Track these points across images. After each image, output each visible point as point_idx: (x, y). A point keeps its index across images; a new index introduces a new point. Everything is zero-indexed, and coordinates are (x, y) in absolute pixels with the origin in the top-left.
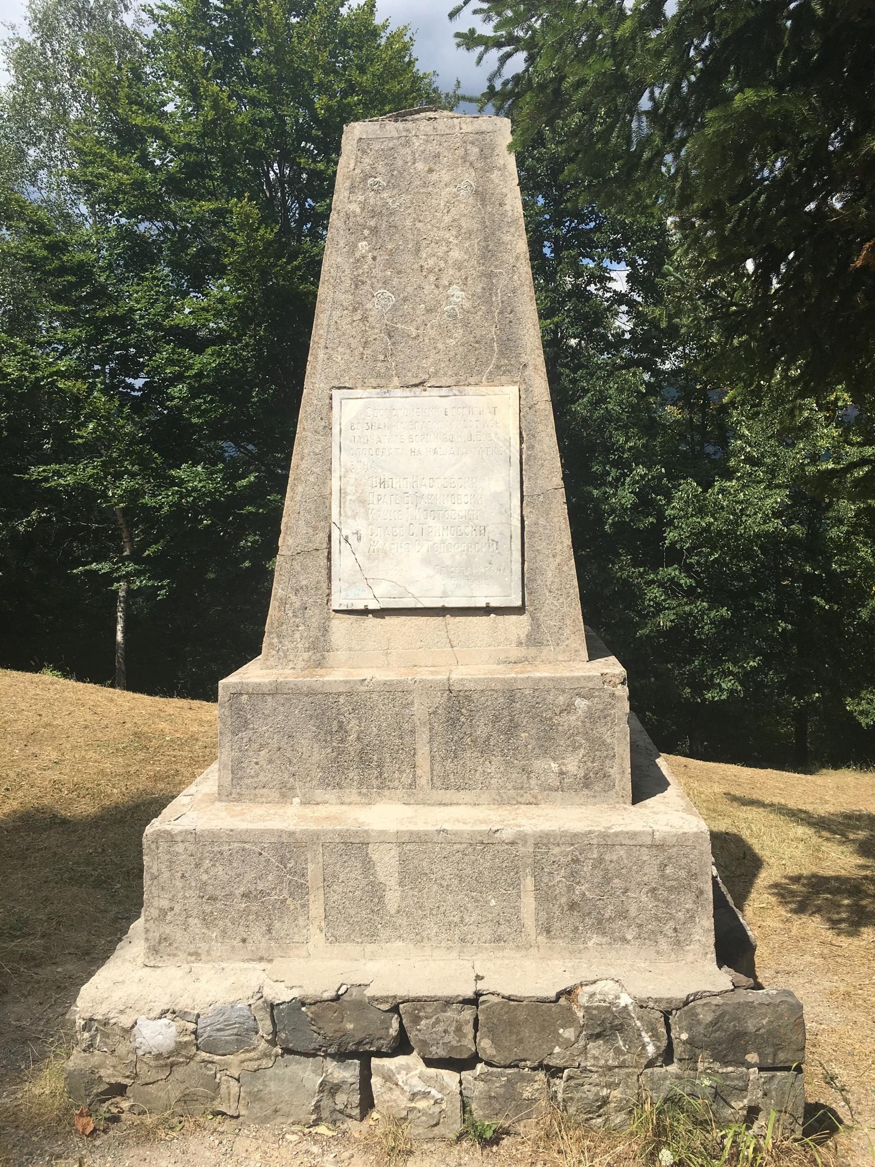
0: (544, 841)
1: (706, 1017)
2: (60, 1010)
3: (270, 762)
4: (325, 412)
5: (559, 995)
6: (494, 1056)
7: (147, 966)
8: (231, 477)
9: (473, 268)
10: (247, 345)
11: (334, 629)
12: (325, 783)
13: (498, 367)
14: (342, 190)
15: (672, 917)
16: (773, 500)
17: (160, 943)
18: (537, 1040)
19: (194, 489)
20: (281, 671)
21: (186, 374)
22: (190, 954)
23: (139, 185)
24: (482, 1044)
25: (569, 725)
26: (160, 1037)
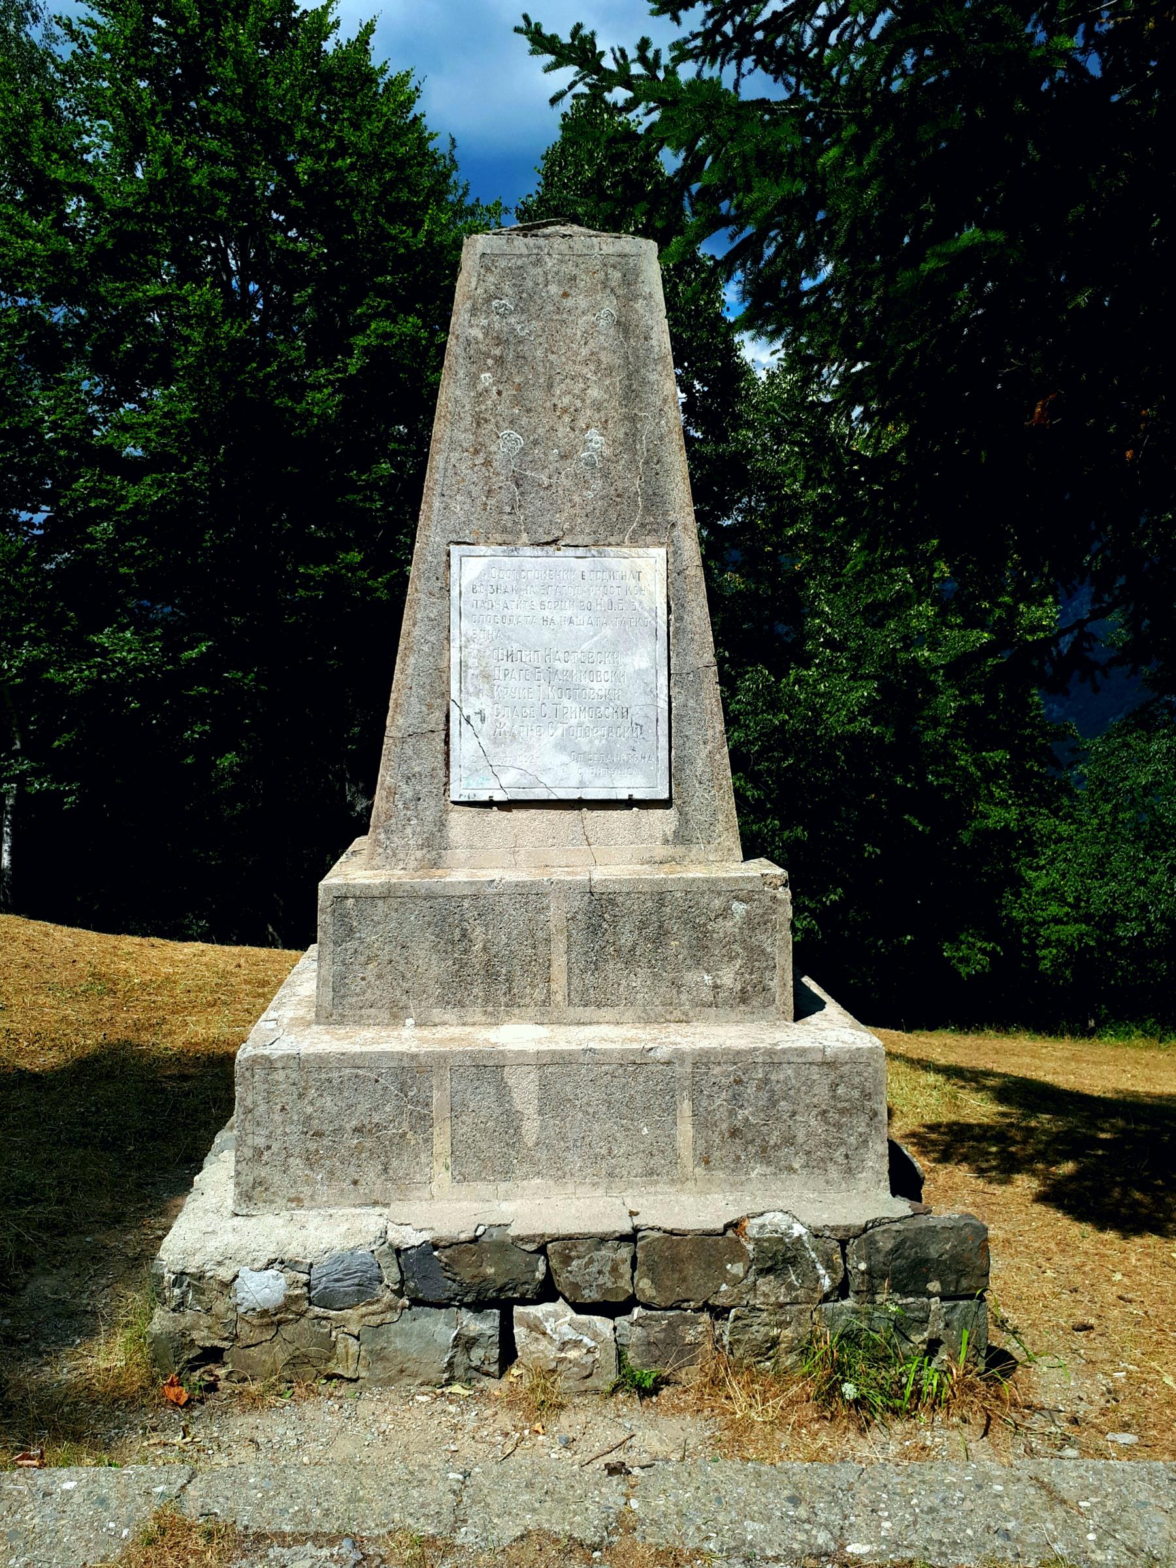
0: (703, 1060)
1: (886, 1244)
2: (103, 1281)
3: (379, 977)
4: (441, 570)
5: (727, 1227)
6: (654, 1298)
7: (237, 1215)
8: (173, 647)
9: (614, 409)
10: (201, 473)
11: (452, 824)
12: (443, 1002)
13: (643, 525)
14: (462, 312)
15: (843, 1143)
16: (860, 694)
17: (253, 1188)
18: (702, 1277)
19: (123, 662)
20: (390, 872)
21: (118, 509)
22: (290, 1200)
23: (58, 258)
24: (641, 1285)
25: (725, 933)
26: (267, 1290)
